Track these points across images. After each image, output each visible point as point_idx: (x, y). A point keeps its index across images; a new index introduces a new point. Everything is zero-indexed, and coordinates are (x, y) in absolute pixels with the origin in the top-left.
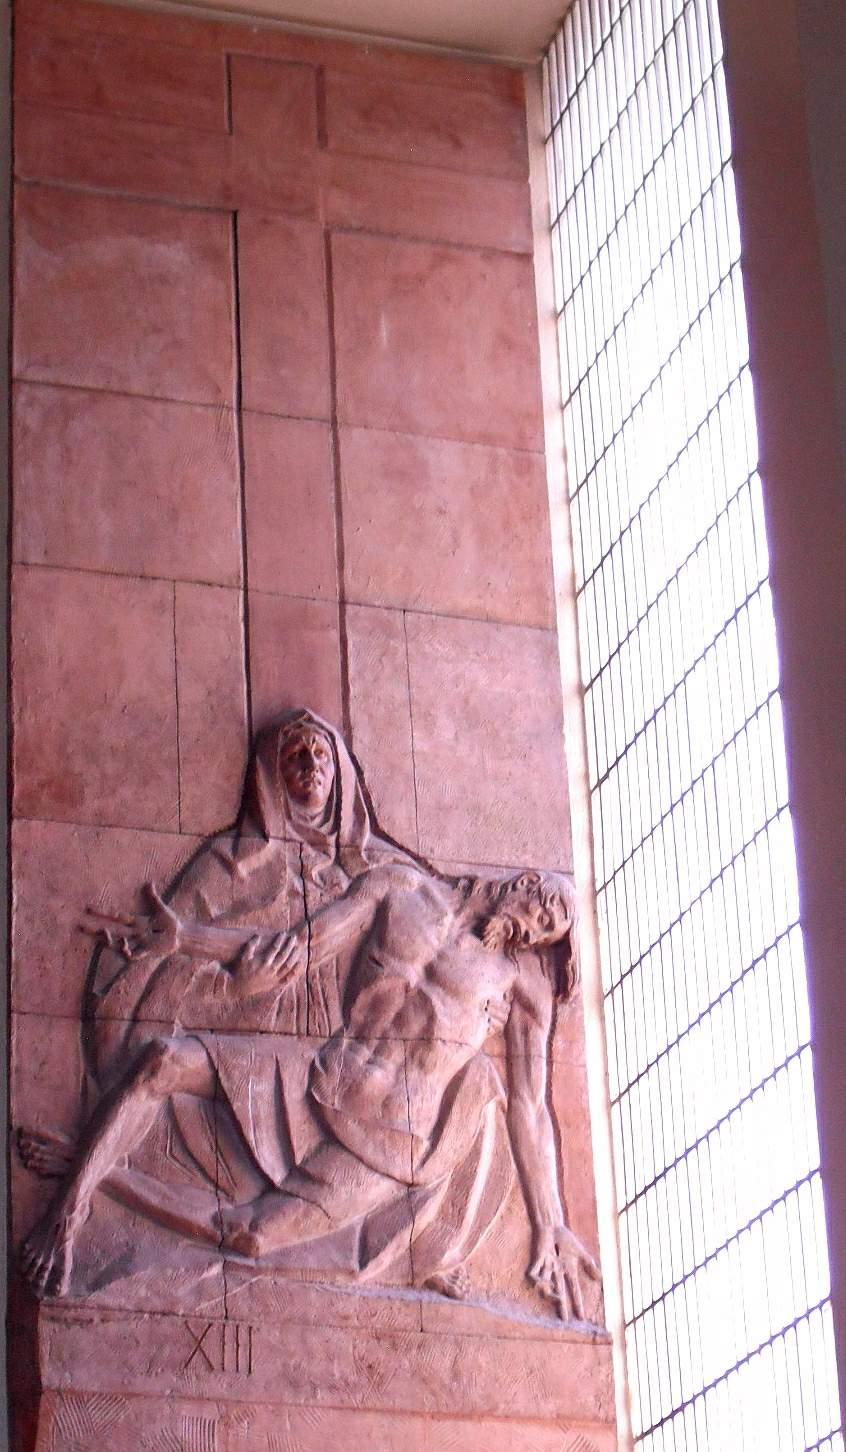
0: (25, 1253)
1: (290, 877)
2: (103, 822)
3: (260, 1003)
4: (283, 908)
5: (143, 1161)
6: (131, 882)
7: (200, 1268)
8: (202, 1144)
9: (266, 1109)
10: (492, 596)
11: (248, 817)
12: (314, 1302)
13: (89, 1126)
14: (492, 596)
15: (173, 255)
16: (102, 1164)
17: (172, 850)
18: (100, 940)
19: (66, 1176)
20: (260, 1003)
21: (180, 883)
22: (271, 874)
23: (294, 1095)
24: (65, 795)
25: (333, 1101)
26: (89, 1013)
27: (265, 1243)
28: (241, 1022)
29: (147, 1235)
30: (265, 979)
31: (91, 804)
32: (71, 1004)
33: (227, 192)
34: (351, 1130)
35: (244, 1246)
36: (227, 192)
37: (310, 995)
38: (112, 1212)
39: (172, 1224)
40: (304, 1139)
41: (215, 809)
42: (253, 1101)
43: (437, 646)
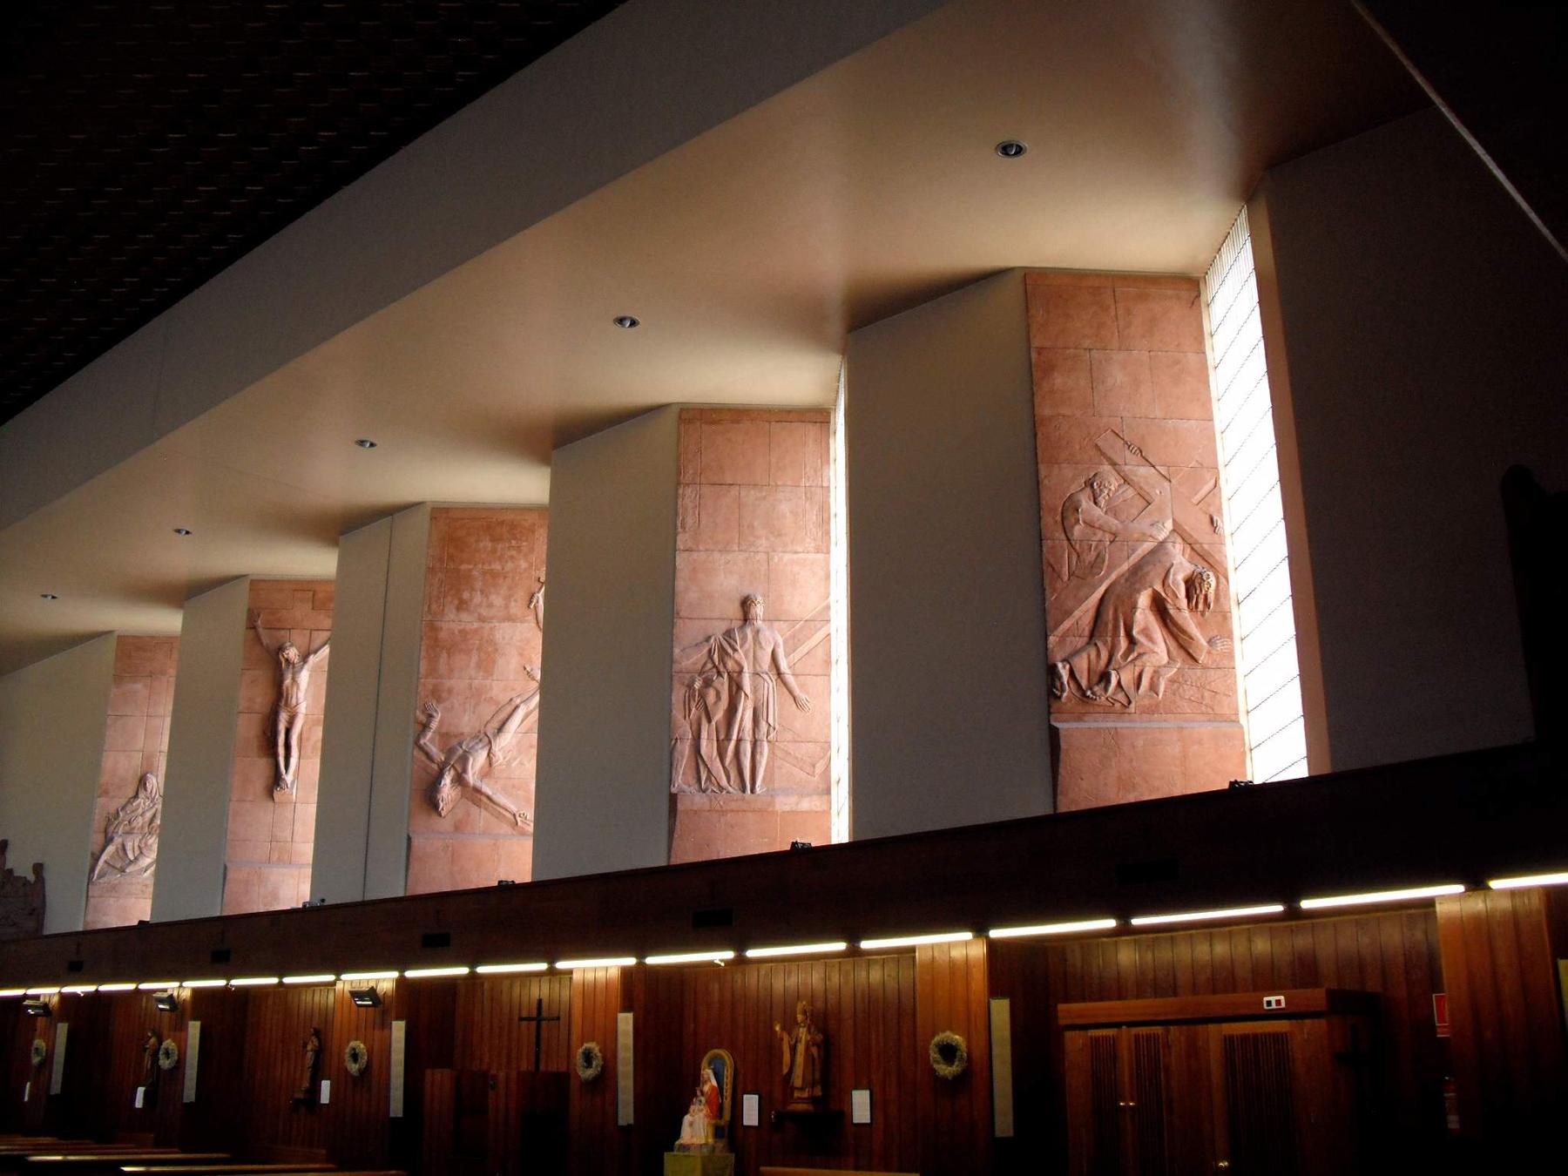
0: (110, 835)
1: (142, 804)
2: (113, 797)
3: (134, 828)
4: (140, 811)
5: (112, 857)
6: (115, 808)
7: (116, 875)
8: (121, 853)
9: (131, 848)
10: (1082, 779)
11: (136, 796)
12: (134, 880)
13: (102, 851)
14: (1082, 779)
15: (139, 686)
16: (104, 857)
17: (123, 801)
18: (109, 820)
19: (97, 860)
20: (134, 828)
21: (123, 808)
22: (139, 805)
23: (136, 844)
24: (106, 793)
25: (143, 845)
26: (106, 832)
27: (127, 870)
28: (130, 833)
29: (110, 869)
30: (134, 824)
31: (111, 794)
32: (102, 830)
33: (151, 672)
34: (144, 851)
35: (124, 871)
36: (151, 672)
37: (142, 827)
38: (106, 866)
39: (113, 867)
40: (137, 853)
41: (131, 793)
42: (129, 846)
43: (487, 1060)
